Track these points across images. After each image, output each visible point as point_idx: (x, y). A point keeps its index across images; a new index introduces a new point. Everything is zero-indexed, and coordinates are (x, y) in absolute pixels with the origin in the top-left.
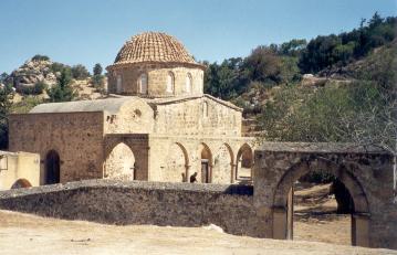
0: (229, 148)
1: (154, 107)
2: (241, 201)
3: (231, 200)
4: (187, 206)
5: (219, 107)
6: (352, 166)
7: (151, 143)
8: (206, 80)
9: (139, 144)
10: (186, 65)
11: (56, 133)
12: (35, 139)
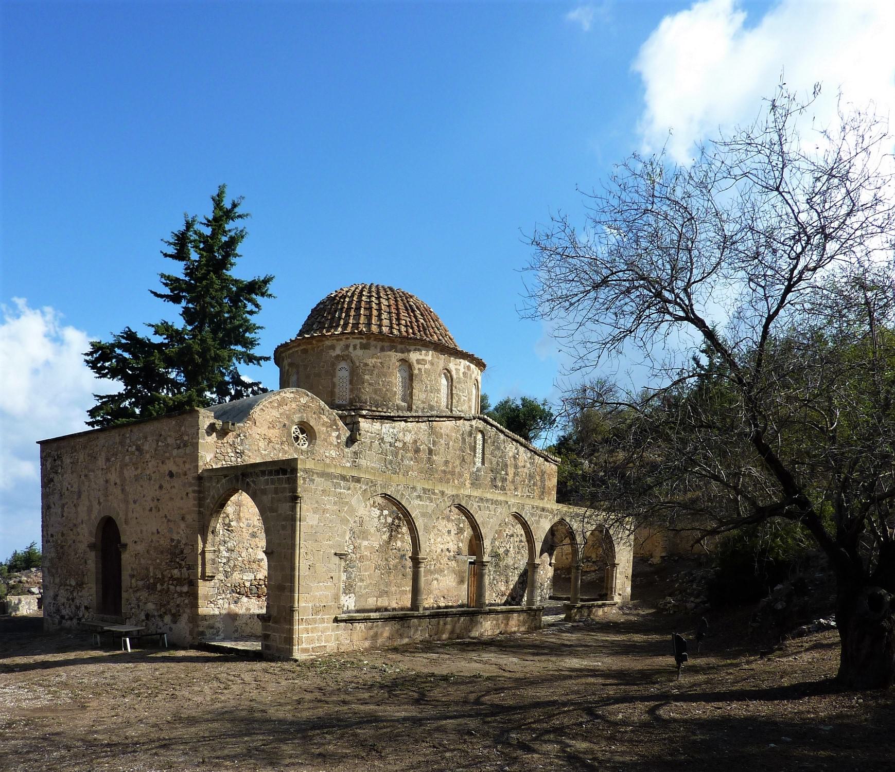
7: (302, 485)
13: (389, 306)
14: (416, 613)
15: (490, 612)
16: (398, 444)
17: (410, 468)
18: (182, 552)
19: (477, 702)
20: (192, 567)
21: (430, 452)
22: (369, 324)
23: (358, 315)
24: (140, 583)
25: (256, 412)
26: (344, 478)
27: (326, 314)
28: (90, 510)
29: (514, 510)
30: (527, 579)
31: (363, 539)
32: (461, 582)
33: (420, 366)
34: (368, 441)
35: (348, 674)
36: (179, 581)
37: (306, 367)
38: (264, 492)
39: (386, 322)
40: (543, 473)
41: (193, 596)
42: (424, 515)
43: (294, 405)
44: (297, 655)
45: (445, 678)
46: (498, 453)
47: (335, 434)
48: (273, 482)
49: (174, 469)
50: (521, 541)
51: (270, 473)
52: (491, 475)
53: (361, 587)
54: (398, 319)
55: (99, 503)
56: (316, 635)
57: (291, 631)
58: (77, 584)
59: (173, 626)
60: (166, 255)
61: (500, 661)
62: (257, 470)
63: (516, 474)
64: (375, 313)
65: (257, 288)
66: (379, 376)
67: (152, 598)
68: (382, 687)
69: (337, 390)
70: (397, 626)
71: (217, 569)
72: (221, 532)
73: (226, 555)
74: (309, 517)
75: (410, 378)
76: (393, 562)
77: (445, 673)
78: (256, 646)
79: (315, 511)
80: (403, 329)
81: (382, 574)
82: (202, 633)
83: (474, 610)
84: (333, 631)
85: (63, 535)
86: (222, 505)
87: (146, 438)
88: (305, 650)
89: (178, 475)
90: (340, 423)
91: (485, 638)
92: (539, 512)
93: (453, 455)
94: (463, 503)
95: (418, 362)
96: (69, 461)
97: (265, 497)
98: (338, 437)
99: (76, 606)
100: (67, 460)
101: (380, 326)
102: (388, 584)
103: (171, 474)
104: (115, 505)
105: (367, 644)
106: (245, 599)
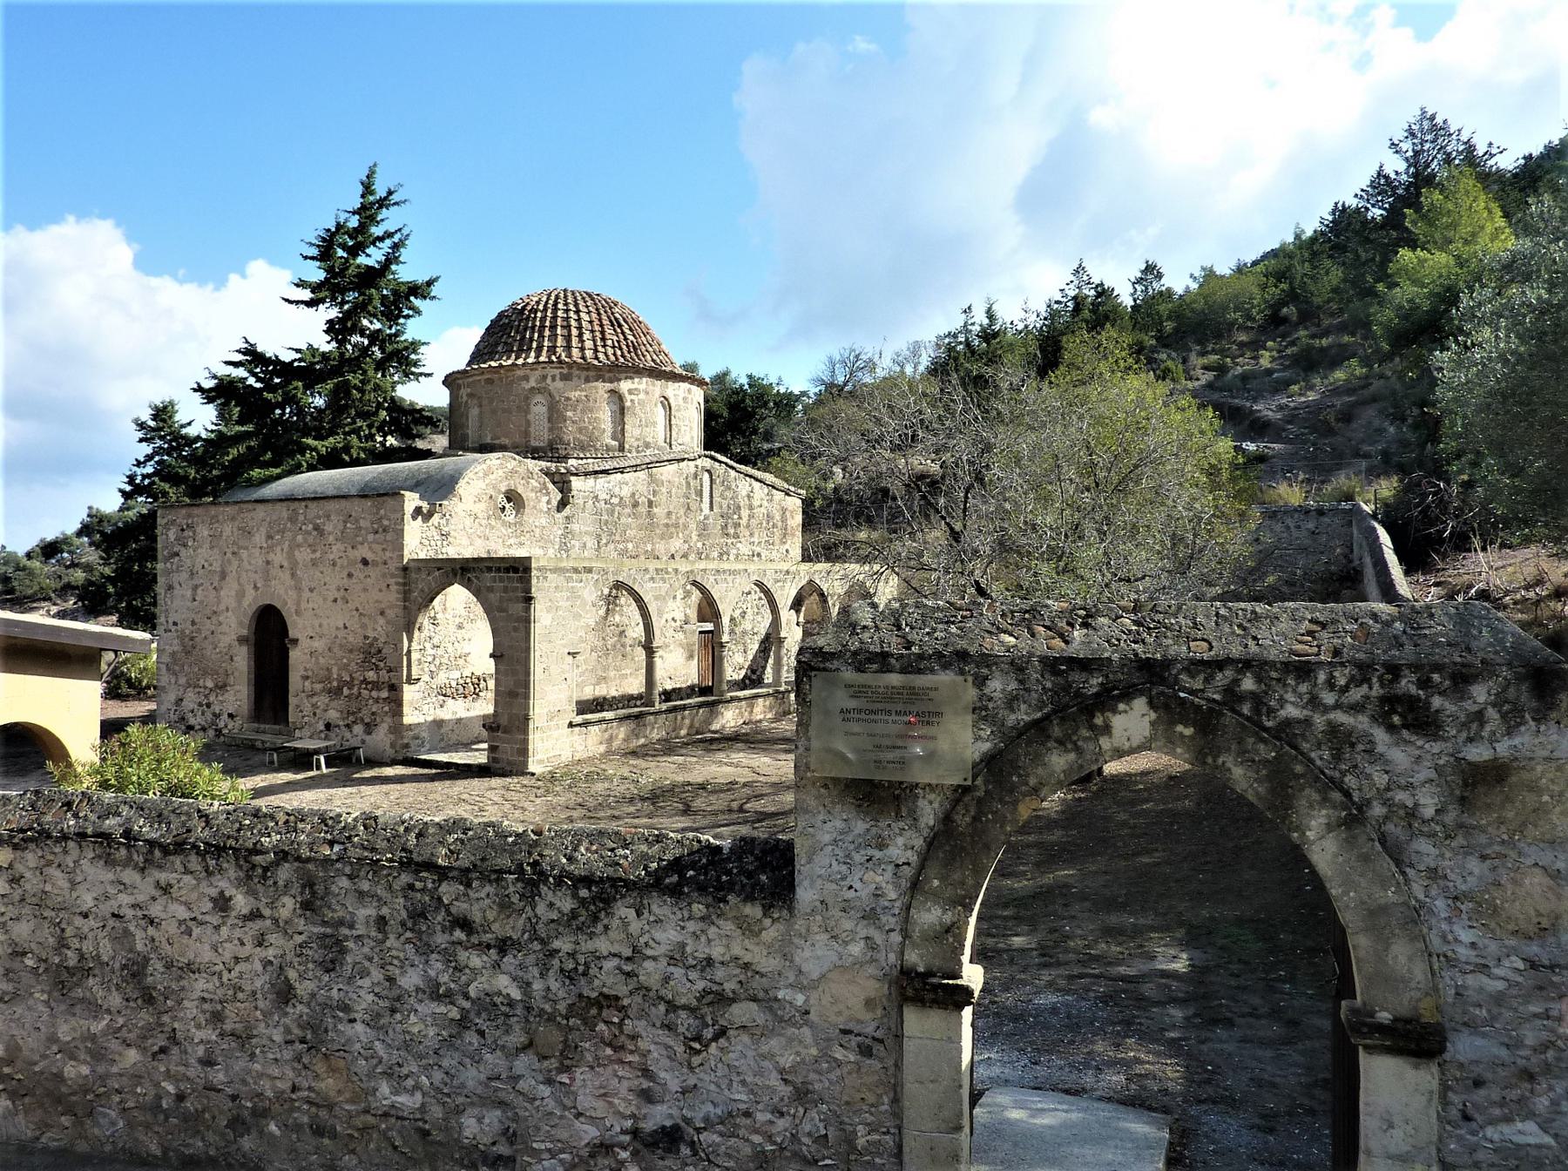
0: (767, 593)
1: (562, 484)
2: (729, 939)
3: (666, 928)
4: (449, 957)
5: (744, 486)
6: (1339, 739)
7: (538, 587)
8: (710, 416)
9: (504, 585)
10: (657, 373)
11: (278, 557)
12: (223, 575)
13: (591, 322)
14: (652, 709)
15: (788, 788)
16: (615, 501)
17: (628, 526)
18: (380, 651)
19: (741, 810)
20: (394, 669)
21: (650, 504)
22: (568, 347)
23: (554, 337)
24: (318, 687)
25: (462, 487)
26: (576, 570)
27: (508, 331)
28: (241, 595)
30: (771, 641)
32: (691, 657)
34: (581, 502)
35: (600, 787)
36: (376, 686)
37: (491, 401)
38: (490, 589)
39: (589, 344)
40: (784, 511)
41: (396, 703)
42: (657, 598)
43: (500, 472)
44: (531, 768)
45: (702, 786)
46: (729, 494)
47: (545, 499)
48: (501, 580)
49: (370, 556)
51: (498, 570)
52: (721, 521)
54: (603, 339)
55: (256, 588)
56: (553, 742)
57: (526, 741)
58: (216, 686)
59: (368, 738)
60: (306, 258)
61: (754, 763)
62: (482, 565)
63: (751, 517)
64: (574, 332)
65: (419, 290)
66: (583, 411)
67: (334, 704)
68: (643, 799)
69: (532, 429)
70: (633, 726)
74: (543, 617)
75: (621, 412)
76: (610, 642)
77: (700, 780)
78: (481, 758)
80: (610, 351)
82: (407, 746)
83: (709, 693)
85: (193, 623)
86: (432, 600)
87: (328, 517)
88: (541, 762)
89: (375, 564)
90: (551, 486)
91: (727, 731)
93: (676, 505)
95: (630, 392)
96: (206, 533)
97: (492, 595)
98: (548, 502)
99: (214, 714)
100: (203, 531)
101: (582, 349)
102: (605, 669)
103: (365, 562)
104: (282, 592)
105: (602, 748)
106: (450, 701)
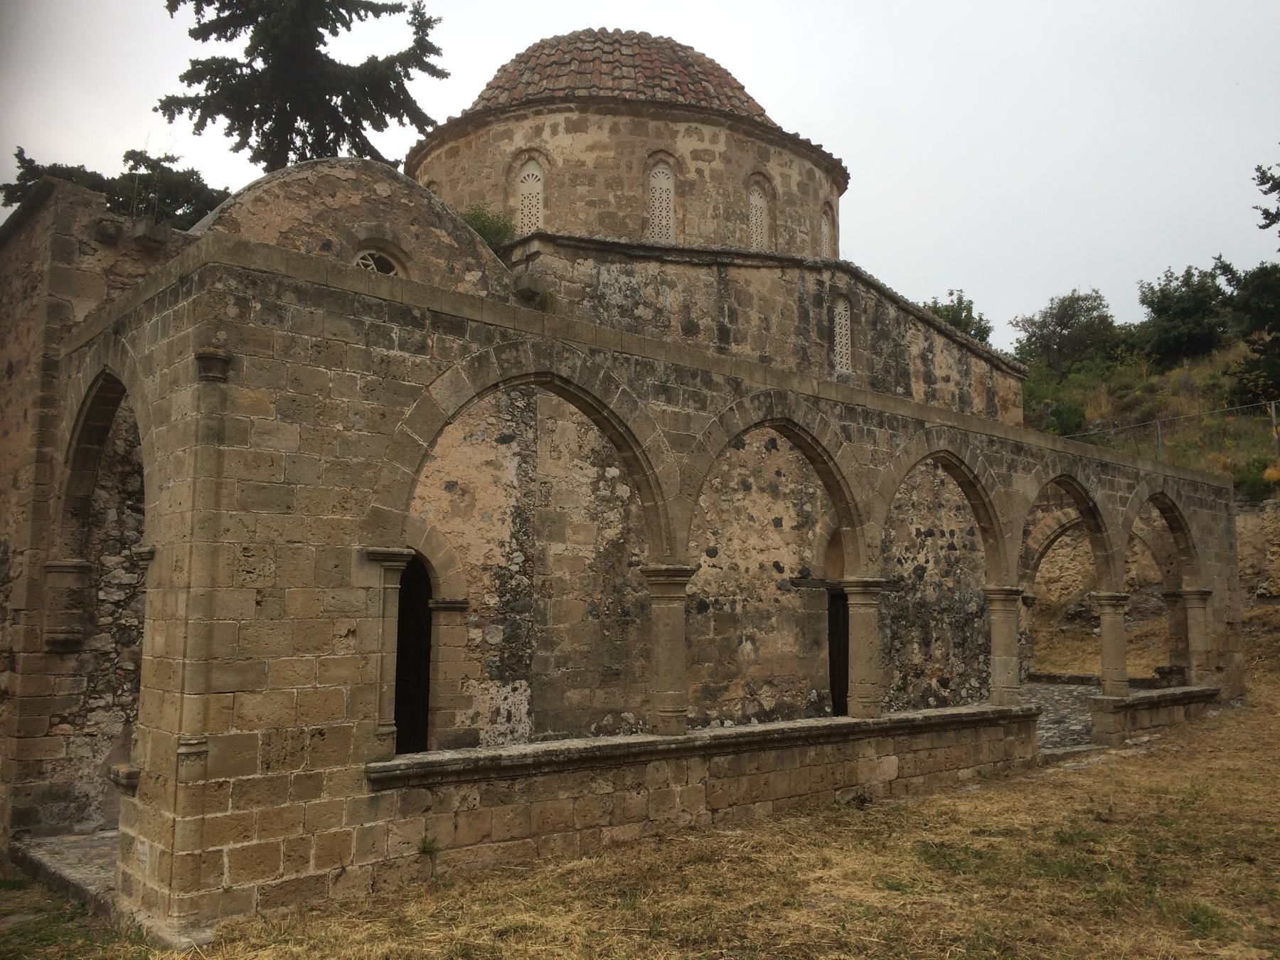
29: (942, 444)
31: (551, 538)
33: (700, 164)
42: (679, 443)
46: (887, 348)
50: (952, 547)
53: (545, 661)
71: (92, 619)
72: (112, 515)
73: (126, 578)
79: (289, 412)
81: (604, 626)
84: (353, 818)
92: (1007, 455)
94: (798, 418)
